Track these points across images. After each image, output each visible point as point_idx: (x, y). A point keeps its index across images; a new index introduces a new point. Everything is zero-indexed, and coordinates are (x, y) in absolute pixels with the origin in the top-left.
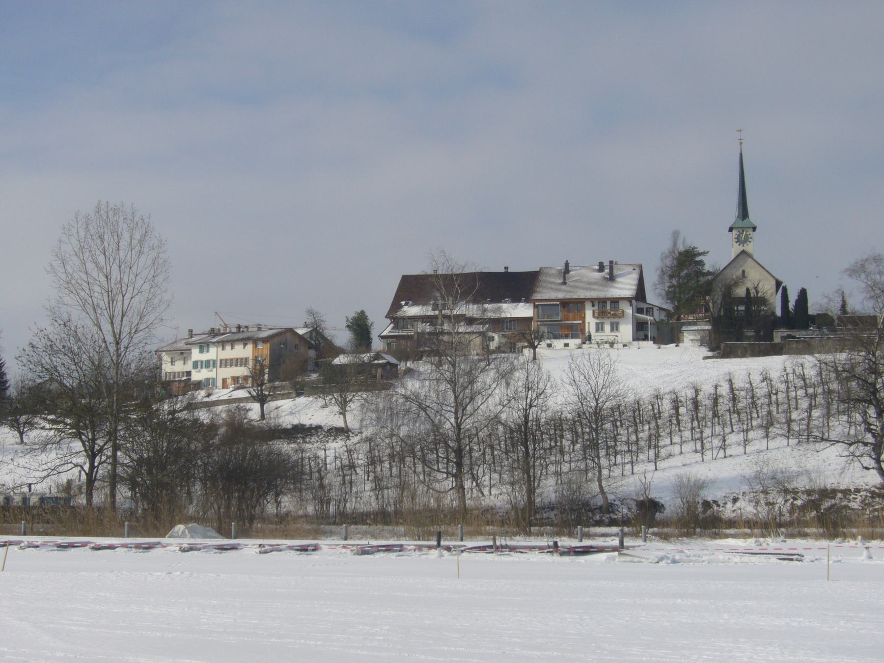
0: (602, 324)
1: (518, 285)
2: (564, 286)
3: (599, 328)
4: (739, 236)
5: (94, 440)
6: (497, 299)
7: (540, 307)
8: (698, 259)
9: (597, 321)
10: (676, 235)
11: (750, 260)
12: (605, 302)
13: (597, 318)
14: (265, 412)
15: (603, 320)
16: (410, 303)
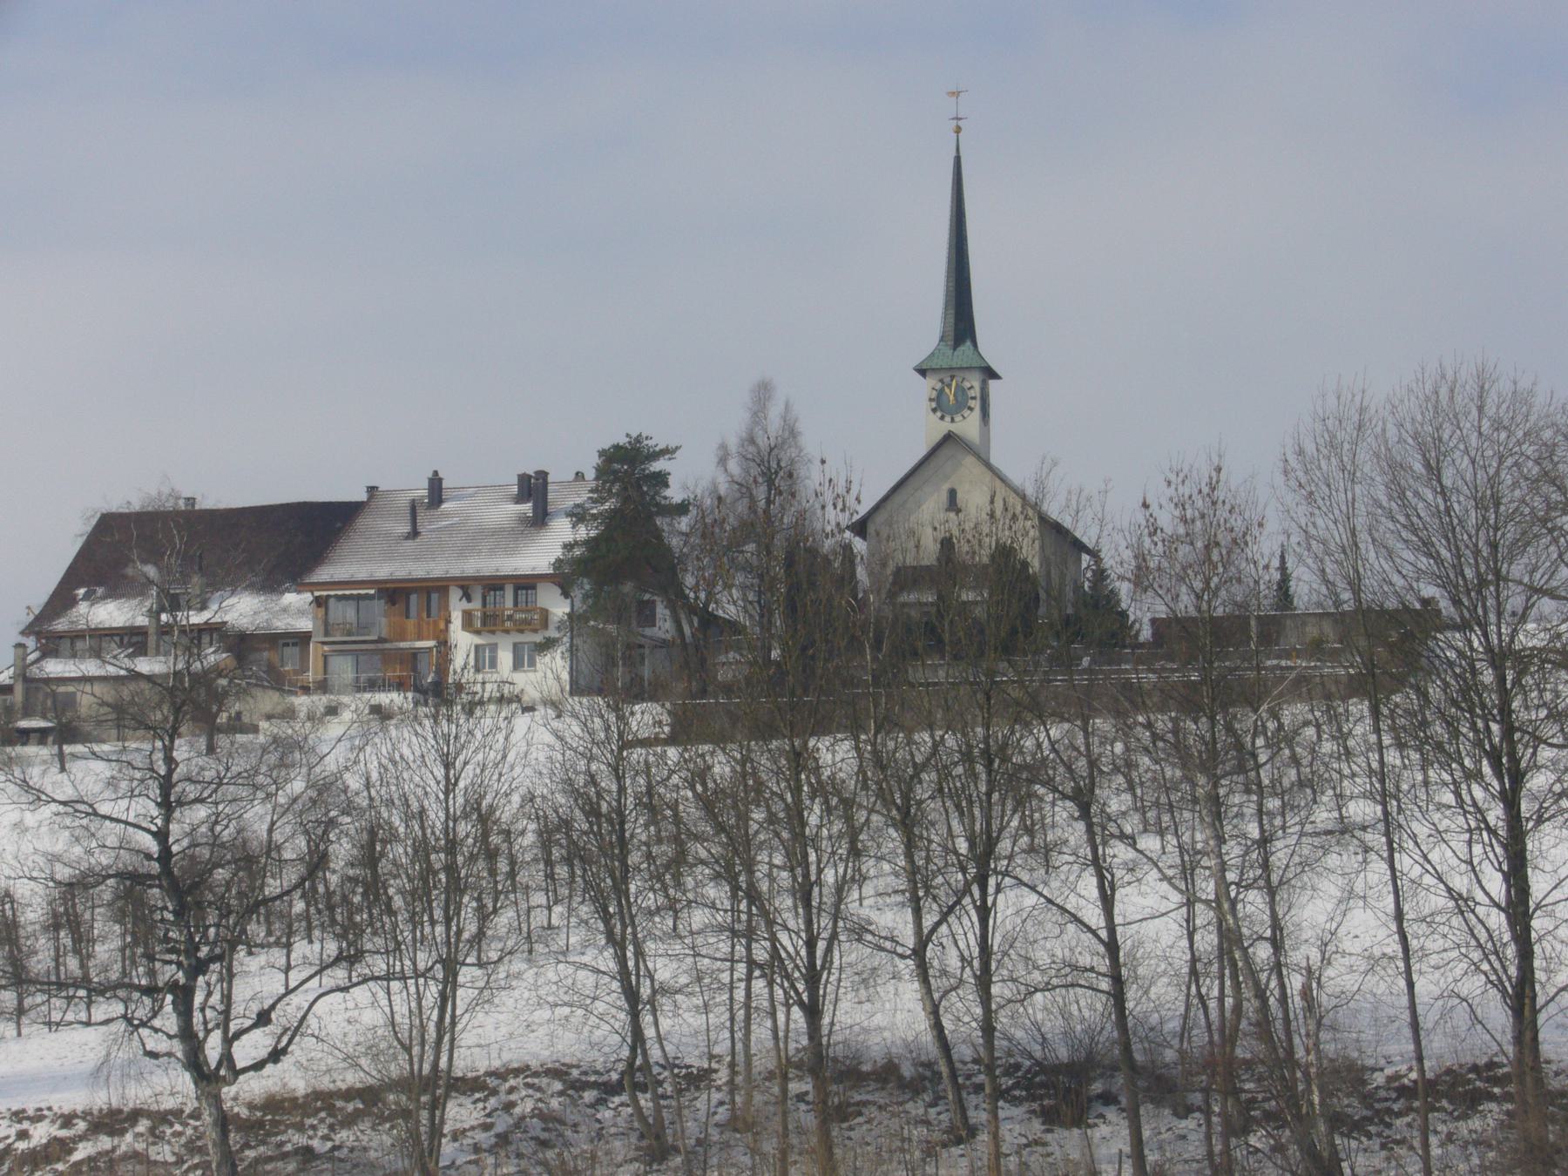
0: (494, 648)
1: (295, 538)
2: (410, 543)
3: (484, 659)
4: (941, 392)
5: (1319, 1059)
6: (225, 579)
7: (332, 602)
8: (657, 466)
9: (478, 640)
10: (763, 392)
11: (970, 460)
12: (502, 588)
13: (478, 632)
14: (996, 942)
15: (491, 639)
16: (100, 591)
